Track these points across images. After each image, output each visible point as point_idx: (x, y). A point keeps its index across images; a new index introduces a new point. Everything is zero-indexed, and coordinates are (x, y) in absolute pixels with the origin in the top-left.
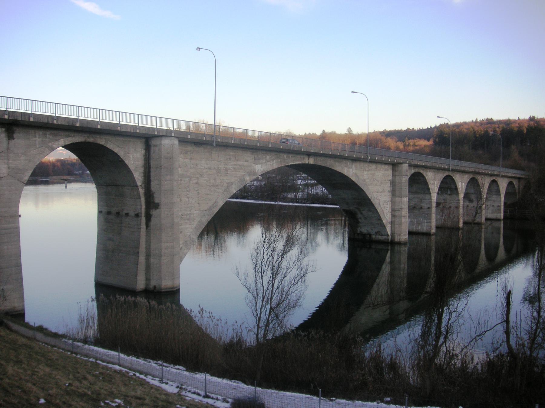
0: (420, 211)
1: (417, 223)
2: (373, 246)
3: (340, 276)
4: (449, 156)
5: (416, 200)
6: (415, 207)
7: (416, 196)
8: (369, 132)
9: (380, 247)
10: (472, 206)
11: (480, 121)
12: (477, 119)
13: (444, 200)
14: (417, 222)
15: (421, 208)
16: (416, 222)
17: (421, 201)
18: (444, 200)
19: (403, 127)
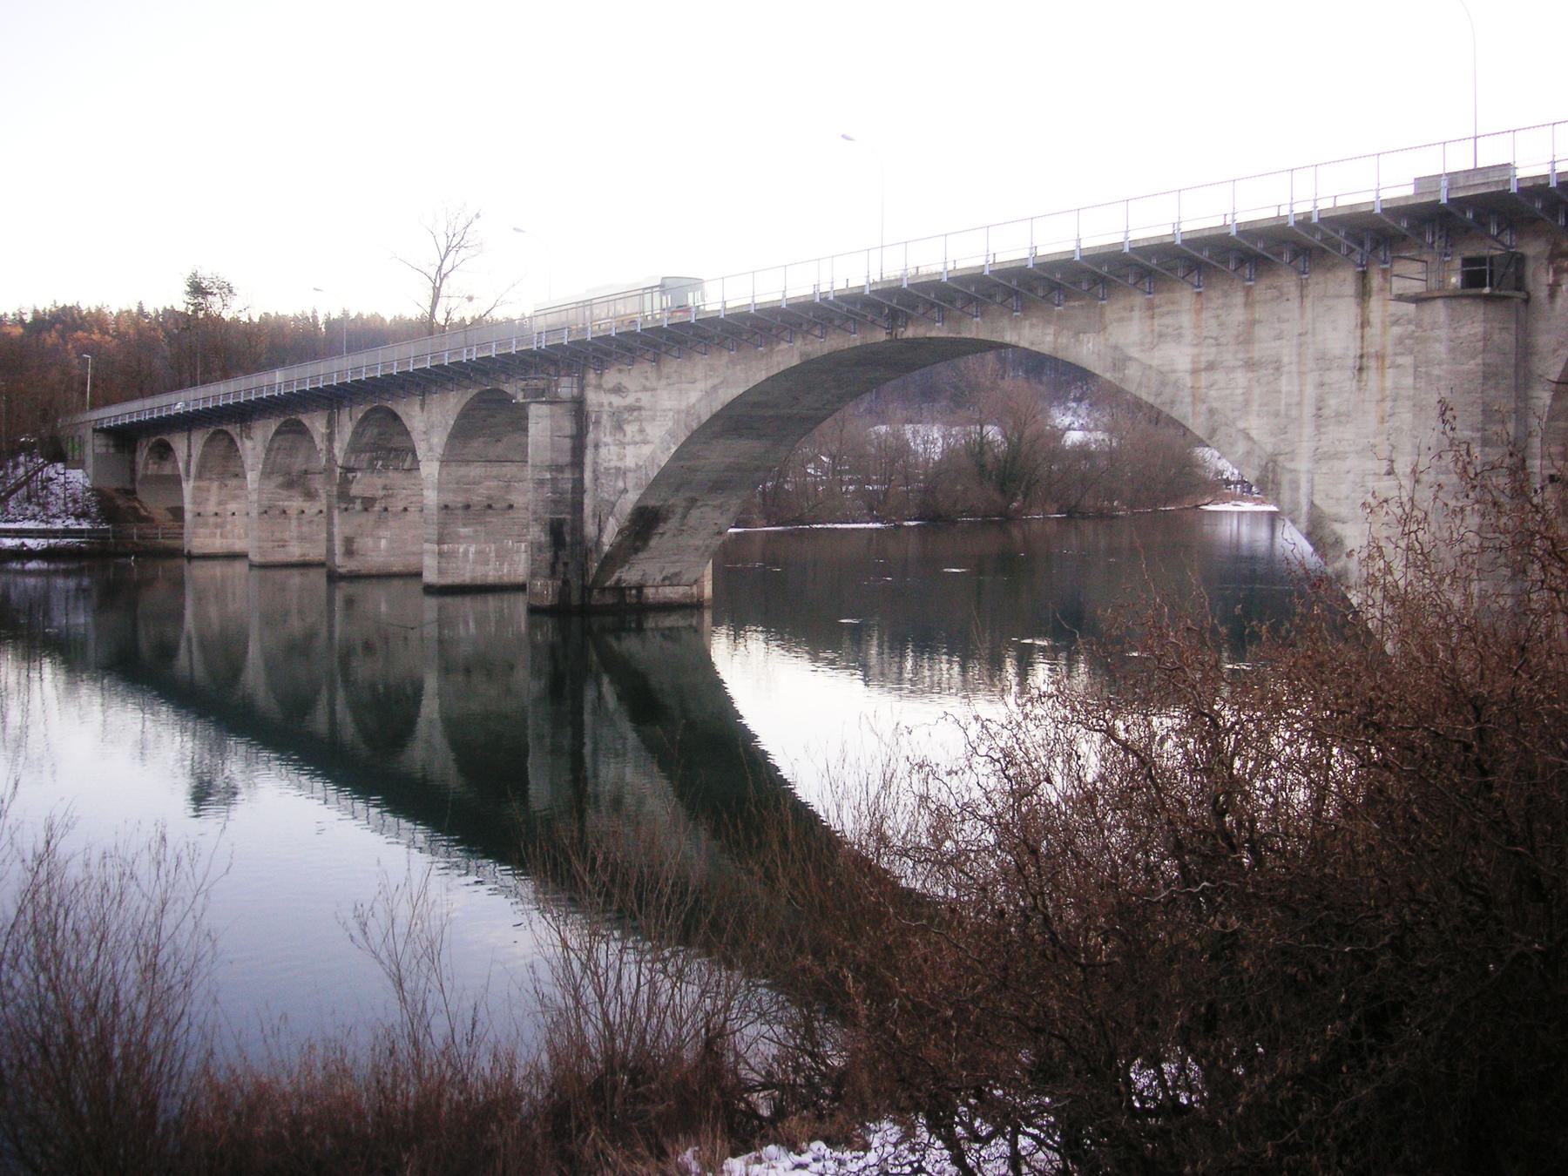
0: (507, 516)
1: (497, 556)
2: (650, 623)
3: (729, 700)
4: (1480, 270)
5: (493, 484)
6: (490, 507)
7: (495, 470)
8: (884, 276)
9: (670, 621)
10: (315, 510)
11: (90, 313)
12: (140, 303)
13: (385, 488)
14: (497, 551)
15: (511, 507)
16: (493, 555)
17: (508, 488)
18: (385, 488)
19: (1491, 165)
